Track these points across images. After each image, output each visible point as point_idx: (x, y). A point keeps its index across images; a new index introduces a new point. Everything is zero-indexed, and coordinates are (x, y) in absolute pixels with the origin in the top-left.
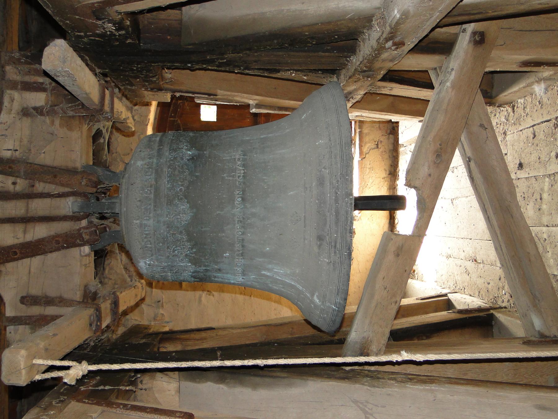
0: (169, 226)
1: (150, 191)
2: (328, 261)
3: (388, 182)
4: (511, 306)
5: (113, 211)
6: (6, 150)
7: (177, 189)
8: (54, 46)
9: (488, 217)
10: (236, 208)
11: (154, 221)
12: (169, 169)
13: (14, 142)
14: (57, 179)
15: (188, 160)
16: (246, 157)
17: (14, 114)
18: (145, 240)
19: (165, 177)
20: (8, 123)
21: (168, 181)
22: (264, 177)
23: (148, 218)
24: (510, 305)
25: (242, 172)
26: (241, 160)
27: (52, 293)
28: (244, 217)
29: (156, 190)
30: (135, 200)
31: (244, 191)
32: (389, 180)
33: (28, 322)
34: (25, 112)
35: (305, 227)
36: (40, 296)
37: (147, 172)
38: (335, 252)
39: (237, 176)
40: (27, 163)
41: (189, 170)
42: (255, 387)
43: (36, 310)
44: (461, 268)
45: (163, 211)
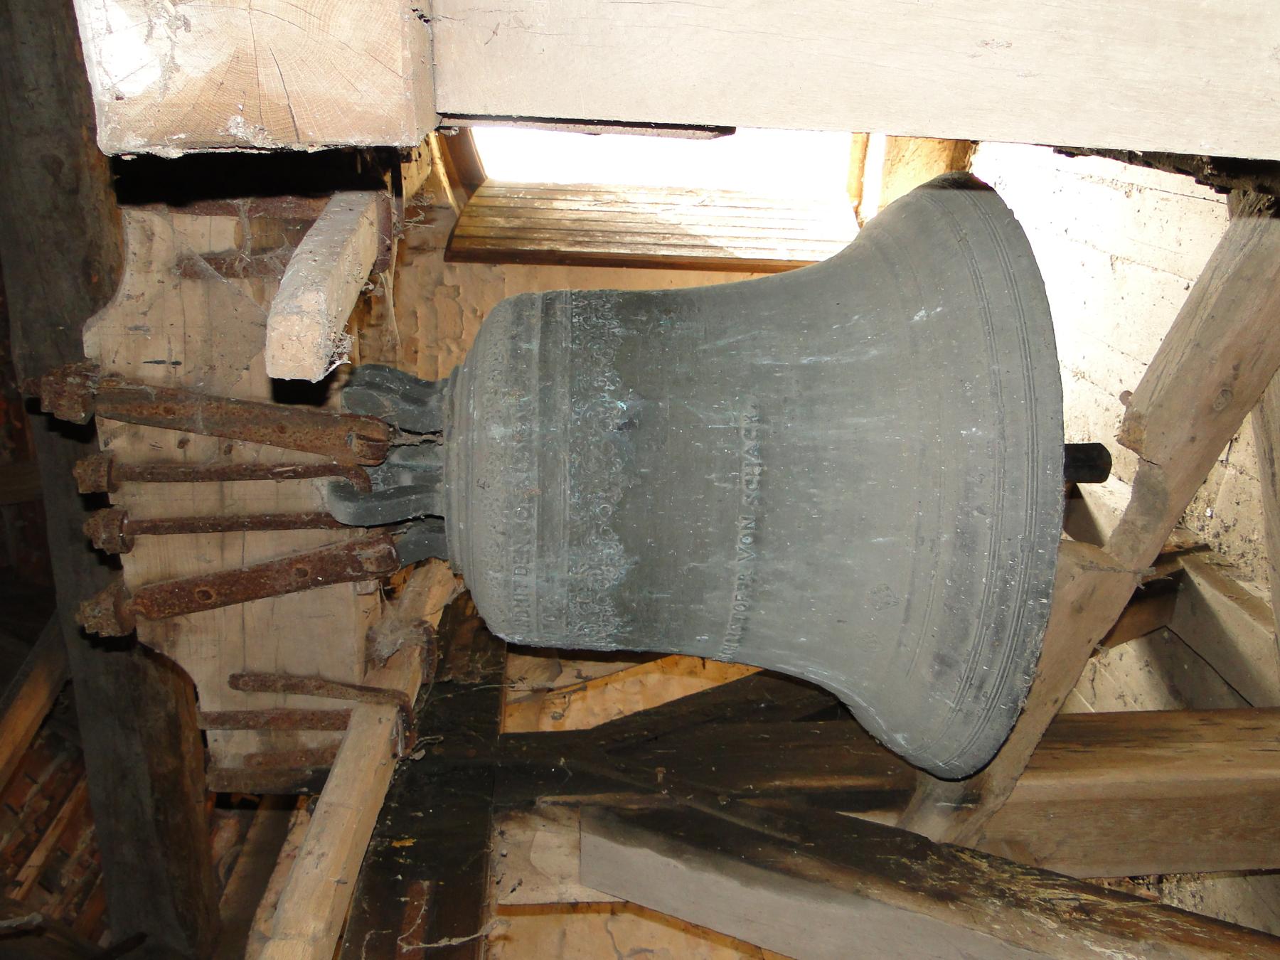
0: (574, 588)
1: (529, 511)
2: (953, 706)
3: (950, 150)
4: (1220, 549)
5: (429, 512)
6: (151, 362)
7: (595, 508)
8: (297, 313)
9: (1273, 475)
10: (737, 559)
11: (537, 577)
12: (574, 455)
13: (169, 343)
14: (287, 435)
15: (620, 429)
16: (766, 427)
17: (158, 272)
18: (517, 609)
19: (565, 475)
20: (147, 296)
21: (572, 488)
22: (812, 490)
23: (524, 572)
24: (1220, 545)
25: (757, 470)
26: (754, 434)
27: (299, 668)
28: (756, 577)
29: (543, 509)
30: (492, 528)
31: (759, 521)
32: (953, 148)
33: (251, 723)
34: (186, 269)
35: (906, 621)
36: (274, 675)
37: (518, 461)
38: (976, 697)
39: (744, 483)
40: (210, 398)
41: (623, 459)
42: (748, 881)
43: (266, 701)
44: (1107, 413)
45: (559, 559)
